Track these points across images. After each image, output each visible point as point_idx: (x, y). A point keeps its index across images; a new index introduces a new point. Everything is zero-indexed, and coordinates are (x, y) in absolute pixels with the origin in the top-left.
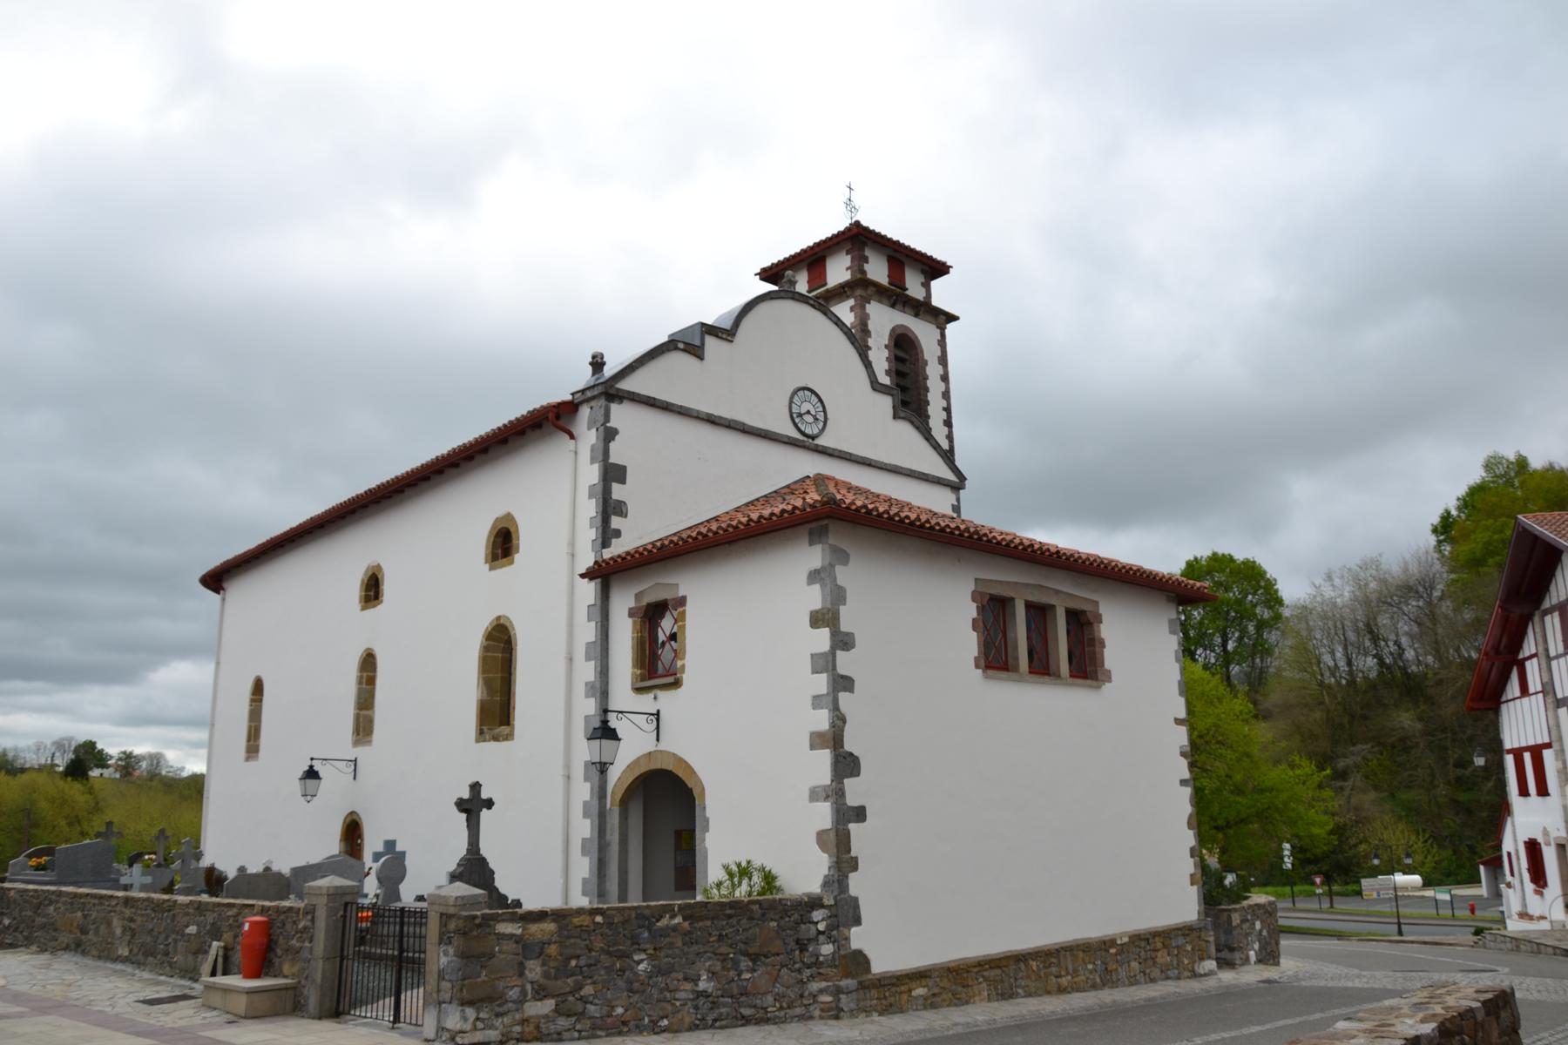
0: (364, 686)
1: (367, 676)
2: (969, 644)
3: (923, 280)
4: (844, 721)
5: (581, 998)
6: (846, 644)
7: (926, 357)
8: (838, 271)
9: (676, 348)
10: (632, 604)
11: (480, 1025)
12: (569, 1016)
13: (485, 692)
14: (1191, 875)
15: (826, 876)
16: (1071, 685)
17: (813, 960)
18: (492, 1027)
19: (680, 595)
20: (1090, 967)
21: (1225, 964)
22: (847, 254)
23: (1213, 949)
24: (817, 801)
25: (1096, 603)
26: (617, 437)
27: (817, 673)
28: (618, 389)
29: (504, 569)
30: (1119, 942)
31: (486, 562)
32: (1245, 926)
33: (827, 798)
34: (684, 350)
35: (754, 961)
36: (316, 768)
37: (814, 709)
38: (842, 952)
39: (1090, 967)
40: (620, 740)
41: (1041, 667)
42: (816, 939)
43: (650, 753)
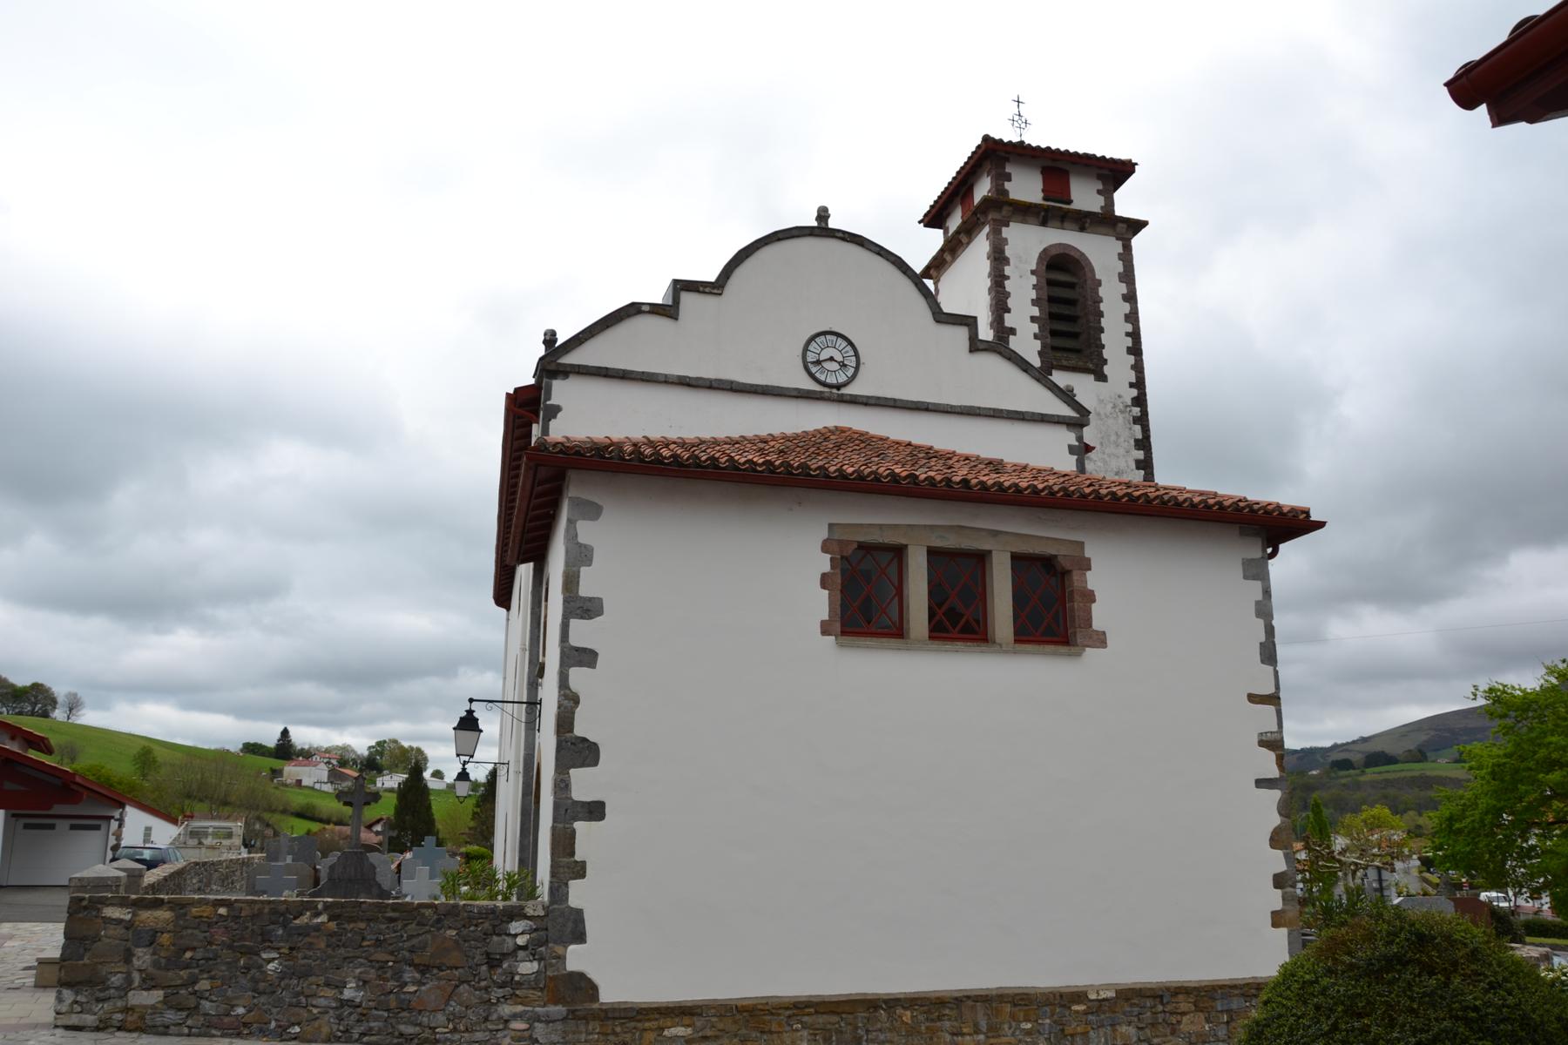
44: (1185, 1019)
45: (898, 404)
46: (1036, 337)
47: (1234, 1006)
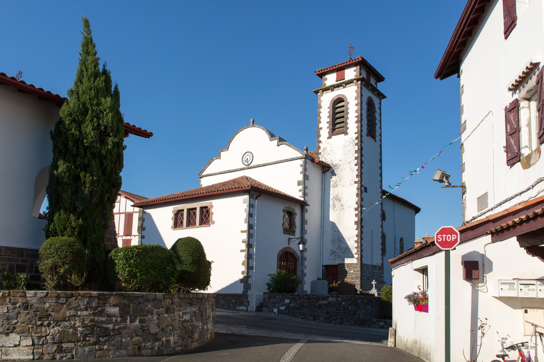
3: (375, 82)
6: (144, 229)
14: (245, 209)
44: (221, 301)
45: (294, 159)
46: (328, 128)
47: (229, 299)
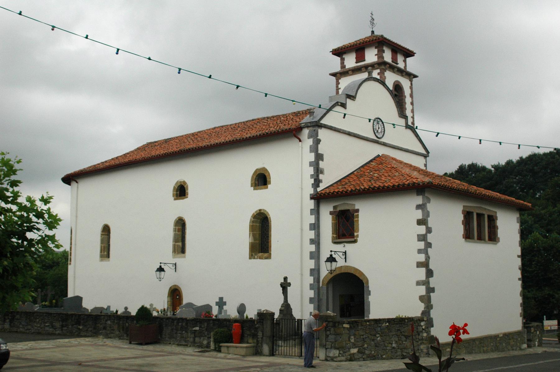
0: (177, 232)
1: (178, 228)
2: (461, 229)
3: (404, 59)
4: (429, 258)
5: (364, 348)
7: (406, 95)
8: (371, 56)
9: (338, 105)
10: (332, 210)
11: (340, 355)
12: (361, 353)
13: (253, 239)
15: (423, 311)
16: (489, 243)
17: (421, 338)
18: (343, 356)
19: (356, 208)
20: (492, 344)
21: (529, 346)
22: (375, 48)
23: (526, 340)
24: (420, 285)
25: (496, 212)
26: (321, 143)
27: (420, 241)
28: (321, 124)
29: (262, 190)
30: (500, 336)
31: (252, 186)
32: (535, 332)
33: (423, 285)
34: (340, 106)
35: (406, 338)
36: (162, 267)
37: (418, 253)
38: (429, 336)
39: (492, 344)
40: (337, 262)
41: (480, 238)
42: (422, 332)
43: (341, 267)
